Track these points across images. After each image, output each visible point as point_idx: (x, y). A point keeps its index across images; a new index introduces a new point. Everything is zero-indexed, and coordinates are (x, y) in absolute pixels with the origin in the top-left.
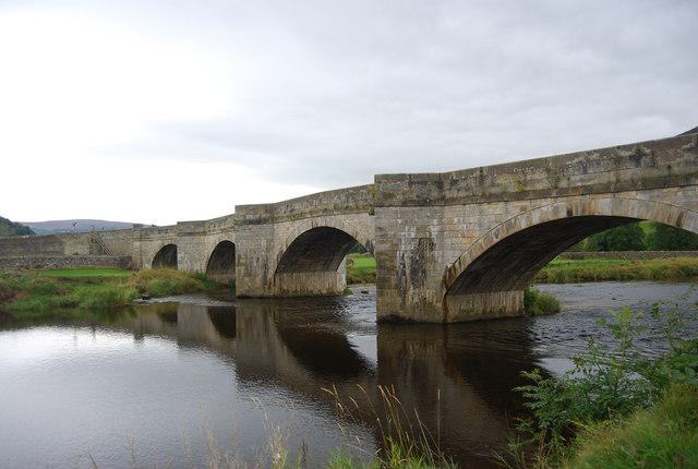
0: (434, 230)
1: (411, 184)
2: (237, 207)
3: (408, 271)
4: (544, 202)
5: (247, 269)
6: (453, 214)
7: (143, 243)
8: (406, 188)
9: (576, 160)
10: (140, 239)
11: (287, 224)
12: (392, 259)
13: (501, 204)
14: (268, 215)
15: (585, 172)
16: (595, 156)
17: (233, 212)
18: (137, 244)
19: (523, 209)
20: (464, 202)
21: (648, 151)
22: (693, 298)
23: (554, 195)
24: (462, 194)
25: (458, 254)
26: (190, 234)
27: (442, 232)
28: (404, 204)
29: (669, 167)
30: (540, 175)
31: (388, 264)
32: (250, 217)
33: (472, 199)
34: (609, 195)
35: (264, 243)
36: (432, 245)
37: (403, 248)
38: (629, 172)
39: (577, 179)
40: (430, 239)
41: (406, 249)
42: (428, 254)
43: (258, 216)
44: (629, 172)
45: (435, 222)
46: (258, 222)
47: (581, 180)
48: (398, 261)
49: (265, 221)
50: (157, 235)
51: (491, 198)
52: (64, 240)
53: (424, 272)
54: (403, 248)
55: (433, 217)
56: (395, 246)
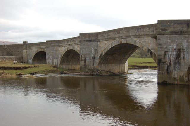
17: (157, 23)
45: (185, 41)
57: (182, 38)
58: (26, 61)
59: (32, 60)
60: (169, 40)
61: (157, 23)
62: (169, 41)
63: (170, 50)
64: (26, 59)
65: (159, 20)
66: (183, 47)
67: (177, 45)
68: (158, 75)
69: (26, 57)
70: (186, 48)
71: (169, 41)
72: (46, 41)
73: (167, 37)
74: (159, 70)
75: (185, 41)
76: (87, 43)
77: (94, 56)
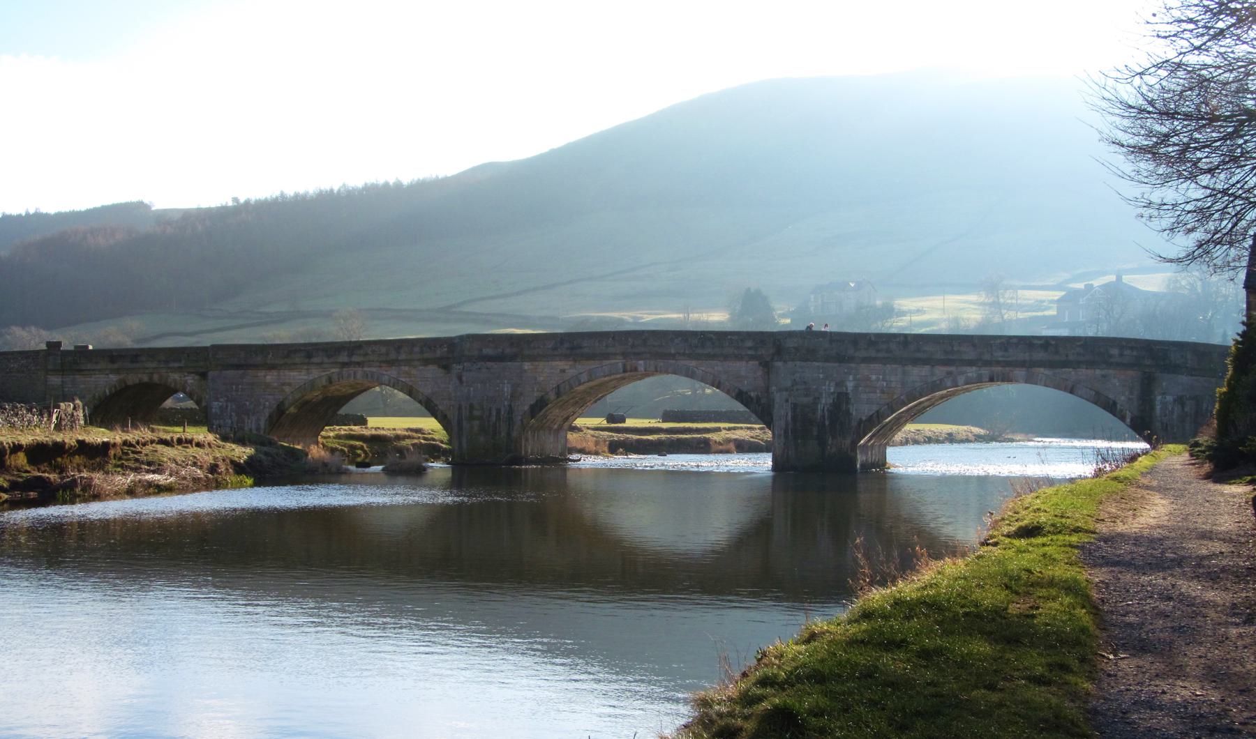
0: (850, 385)
3: (827, 423)
4: (968, 369)
9: (998, 341)
11: (562, 364)
13: (927, 368)
15: (1006, 350)
16: (1015, 341)
19: (949, 373)
20: (885, 361)
21: (1053, 343)
22: (1254, 215)
24: (880, 355)
25: (875, 408)
26: (238, 367)
27: (856, 387)
28: (827, 360)
29: (1067, 356)
30: (1115, 352)
32: (488, 351)
34: (1024, 369)
35: (507, 389)
36: (848, 398)
37: (823, 401)
38: (1040, 355)
39: (999, 355)
40: (847, 394)
41: (826, 401)
43: (500, 350)
44: (1040, 355)
45: (851, 378)
47: (1002, 356)
48: (819, 412)
49: (512, 358)
51: (916, 362)
54: (823, 401)
56: (817, 400)
57: (846, 371)
60: (822, 373)
62: (821, 376)
63: (824, 395)
66: (847, 389)
67: (837, 385)
71: (821, 376)
75: (851, 378)
76: (489, 364)
77: (510, 406)
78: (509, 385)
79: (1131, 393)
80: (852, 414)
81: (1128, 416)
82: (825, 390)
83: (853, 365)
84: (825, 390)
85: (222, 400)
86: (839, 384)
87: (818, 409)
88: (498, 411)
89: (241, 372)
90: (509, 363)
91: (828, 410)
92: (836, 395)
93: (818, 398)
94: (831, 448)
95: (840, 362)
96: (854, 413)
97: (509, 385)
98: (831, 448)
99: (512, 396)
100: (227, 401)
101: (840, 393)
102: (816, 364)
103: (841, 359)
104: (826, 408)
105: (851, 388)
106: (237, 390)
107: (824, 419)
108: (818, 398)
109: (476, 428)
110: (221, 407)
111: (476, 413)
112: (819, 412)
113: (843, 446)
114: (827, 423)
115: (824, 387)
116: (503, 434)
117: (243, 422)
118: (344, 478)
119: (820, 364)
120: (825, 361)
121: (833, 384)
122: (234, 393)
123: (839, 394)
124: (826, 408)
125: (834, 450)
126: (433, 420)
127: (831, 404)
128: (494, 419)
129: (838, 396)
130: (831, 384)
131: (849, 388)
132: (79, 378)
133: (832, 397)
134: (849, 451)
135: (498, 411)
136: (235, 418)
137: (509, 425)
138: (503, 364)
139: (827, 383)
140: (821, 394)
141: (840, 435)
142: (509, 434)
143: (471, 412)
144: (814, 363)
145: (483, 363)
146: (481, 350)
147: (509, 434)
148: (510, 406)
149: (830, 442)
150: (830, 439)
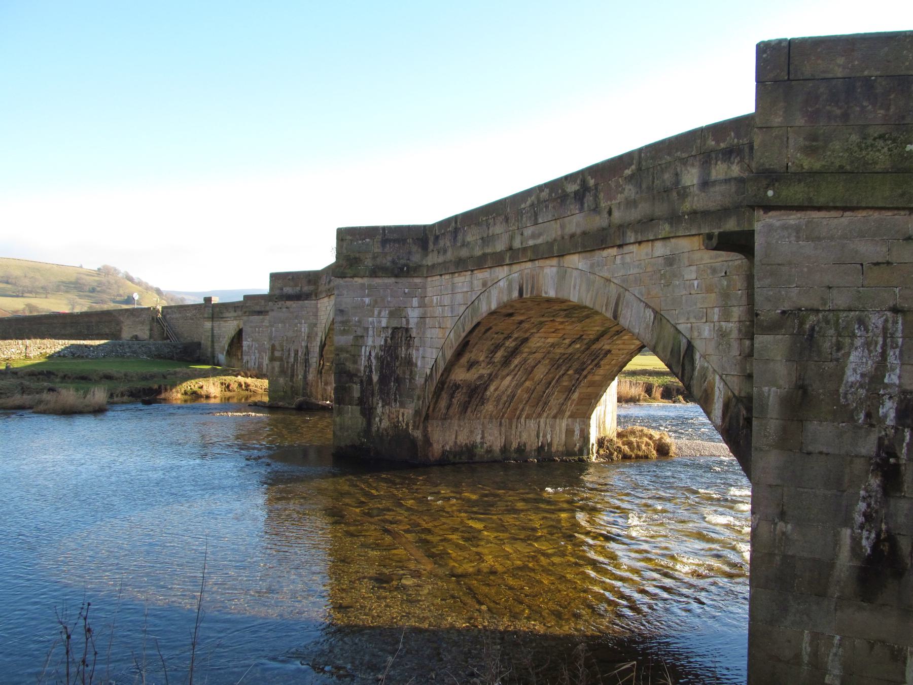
0: (413, 315)
1: (385, 242)
2: (346, 236)
3: (375, 378)
5: (281, 366)
6: (435, 286)
7: (216, 324)
8: (377, 249)
10: (212, 318)
12: (355, 358)
14: (312, 288)
16: (545, 194)
17: (242, 299)
18: (208, 325)
23: (507, 262)
26: (259, 313)
27: (423, 318)
28: (374, 273)
31: (350, 366)
32: (288, 290)
33: (462, 265)
35: (305, 329)
40: (407, 330)
41: (374, 343)
42: (403, 352)
43: (298, 289)
45: (415, 302)
46: (298, 297)
48: (363, 362)
50: (233, 314)
52: (122, 319)
53: (398, 380)
54: (370, 342)
55: (411, 295)
56: (359, 339)
57: (406, 290)
58: (209, 355)
59: (225, 353)
60: (368, 296)
61: (242, 299)
62: (367, 300)
63: (371, 333)
64: (210, 350)
65: (766, 37)
66: (408, 322)
67: (392, 315)
68: (749, 621)
69: (209, 344)
70: (417, 323)
71: (367, 300)
72: (263, 287)
73: (362, 286)
74: (752, 546)
75: (415, 302)
76: (289, 303)
77: (307, 347)
78: (306, 325)
79: (726, 315)
80: (416, 365)
81: (717, 393)
82: (373, 323)
83: (417, 280)
84: (373, 323)
85: (249, 340)
86: (397, 313)
87: (360, 356)
88: (296, 352)
89: (261, 317)
90: (306, 302)
91: (377, 357)
92: (390, 331)
93: (362, 337)
94: (381, 421)
95: (396, 276)
96: (419, 364)
97: (306, 325)
98: (381, 421)
99: (308, 337)
100: (252, 341)
101: (396, 328)
102: (359, 280)
103: (401, 271)
104: (373, 354)
105: (416, 320)
106: (259, 333)
107: (371, 371)
108: (362, 337)
109: (277, 369)
110: (248, 346)
111: (277, 354)
112: (363, 362)
113: (401, 418)
114: (375, 378)
115: (370, 319)
116: (300, 377)
117: (263, 358)
118: (709, 391)
119: (366, 281)
120: (371, 276)
121: (385, 313)
122: (257, 334)
123: (395, 329)
124: (373, 354)
125: (385, 424)
126: (656, 358)
127: (381, 346)
128: (292, 360)
129: (393, 333)
130: (383, 314)
131: (411, 321)
132: (223, 324)
133: (383, 335)
134: (411, 428)
135: (296, 352)
136: (257, 355)
137: (306, 367)
138: (300, 302)
139: (376, 313)
140: (367, 329)
141: (395, 401)
142: (305, 377)
143: (273, 353)
144: (356, 279)
145: (283, 302)
146: (282, 289)
147: (305, 377)
148: (307, 347)
149: (379, 410)
150: (380, 405)
